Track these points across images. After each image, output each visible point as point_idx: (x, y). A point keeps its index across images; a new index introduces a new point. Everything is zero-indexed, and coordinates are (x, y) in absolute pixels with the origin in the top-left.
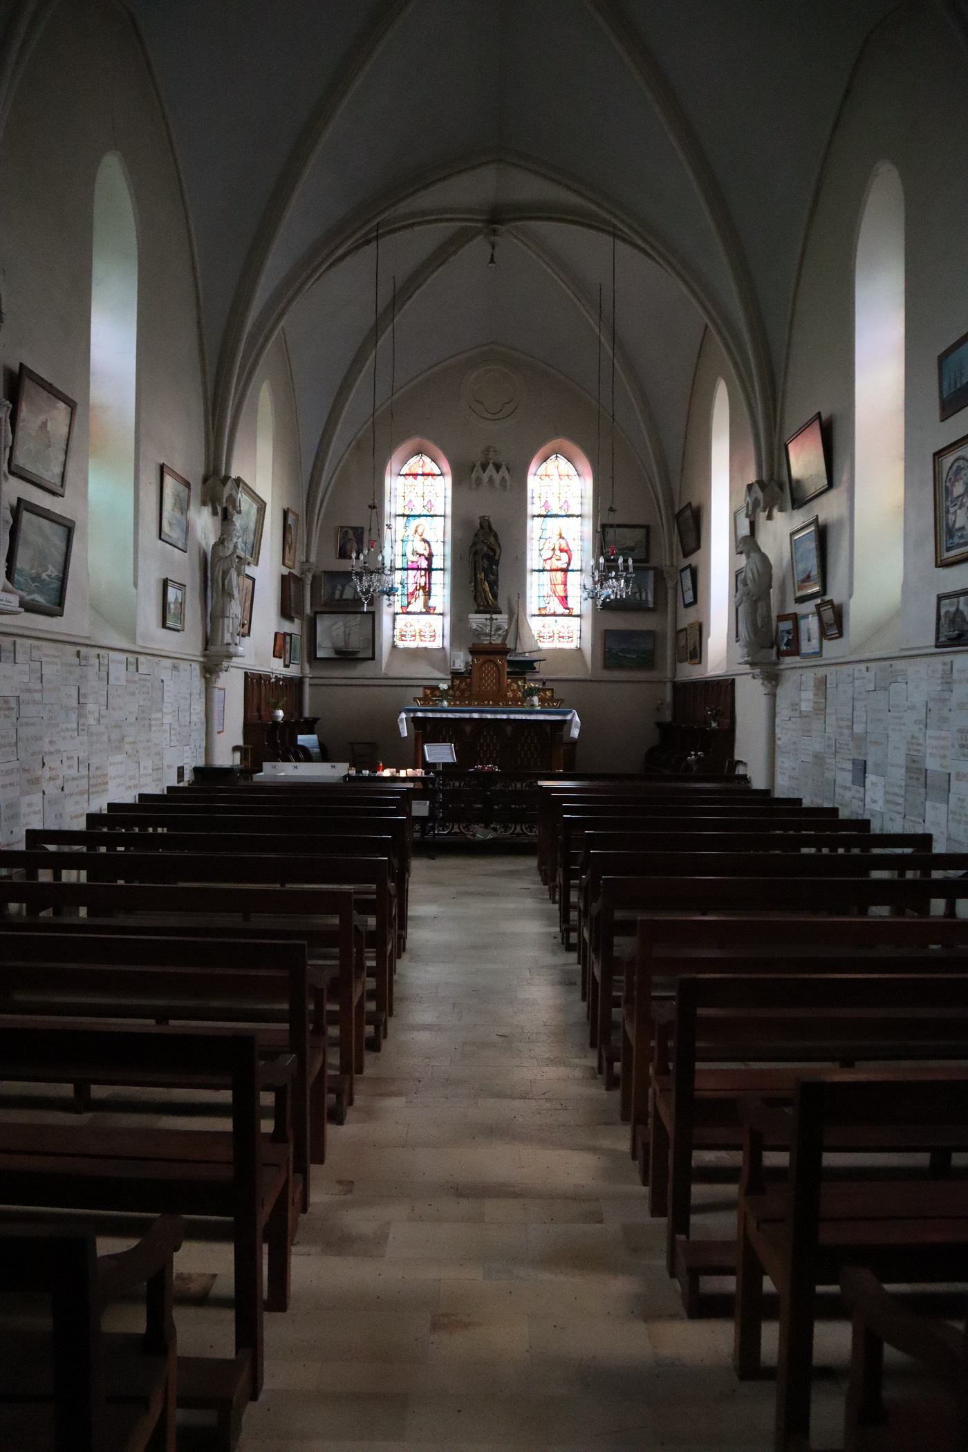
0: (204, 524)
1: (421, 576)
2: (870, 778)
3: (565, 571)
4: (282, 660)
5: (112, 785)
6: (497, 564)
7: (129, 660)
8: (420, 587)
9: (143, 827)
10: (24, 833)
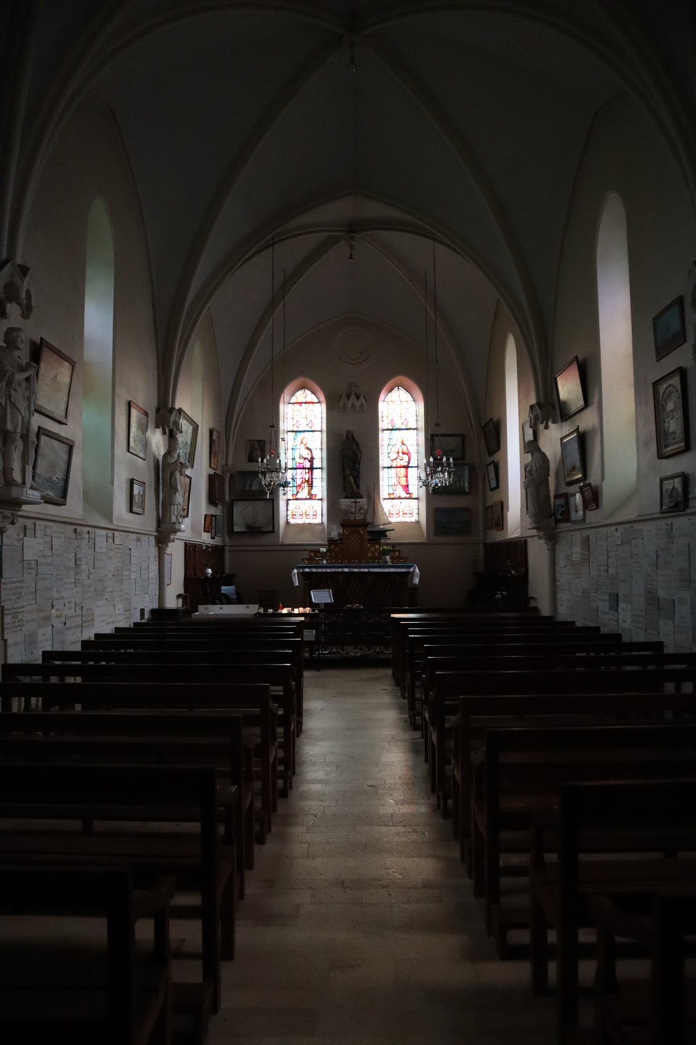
0: (157, 440)
1: (306, 473)
2: (622, 605)
3: (407, 467)
4: (210, 534)
5: (97, 621)
6: (359, 463)
7: (108, 535)
8: (305, 481)
9: (125, 650)
10: (41, 654)
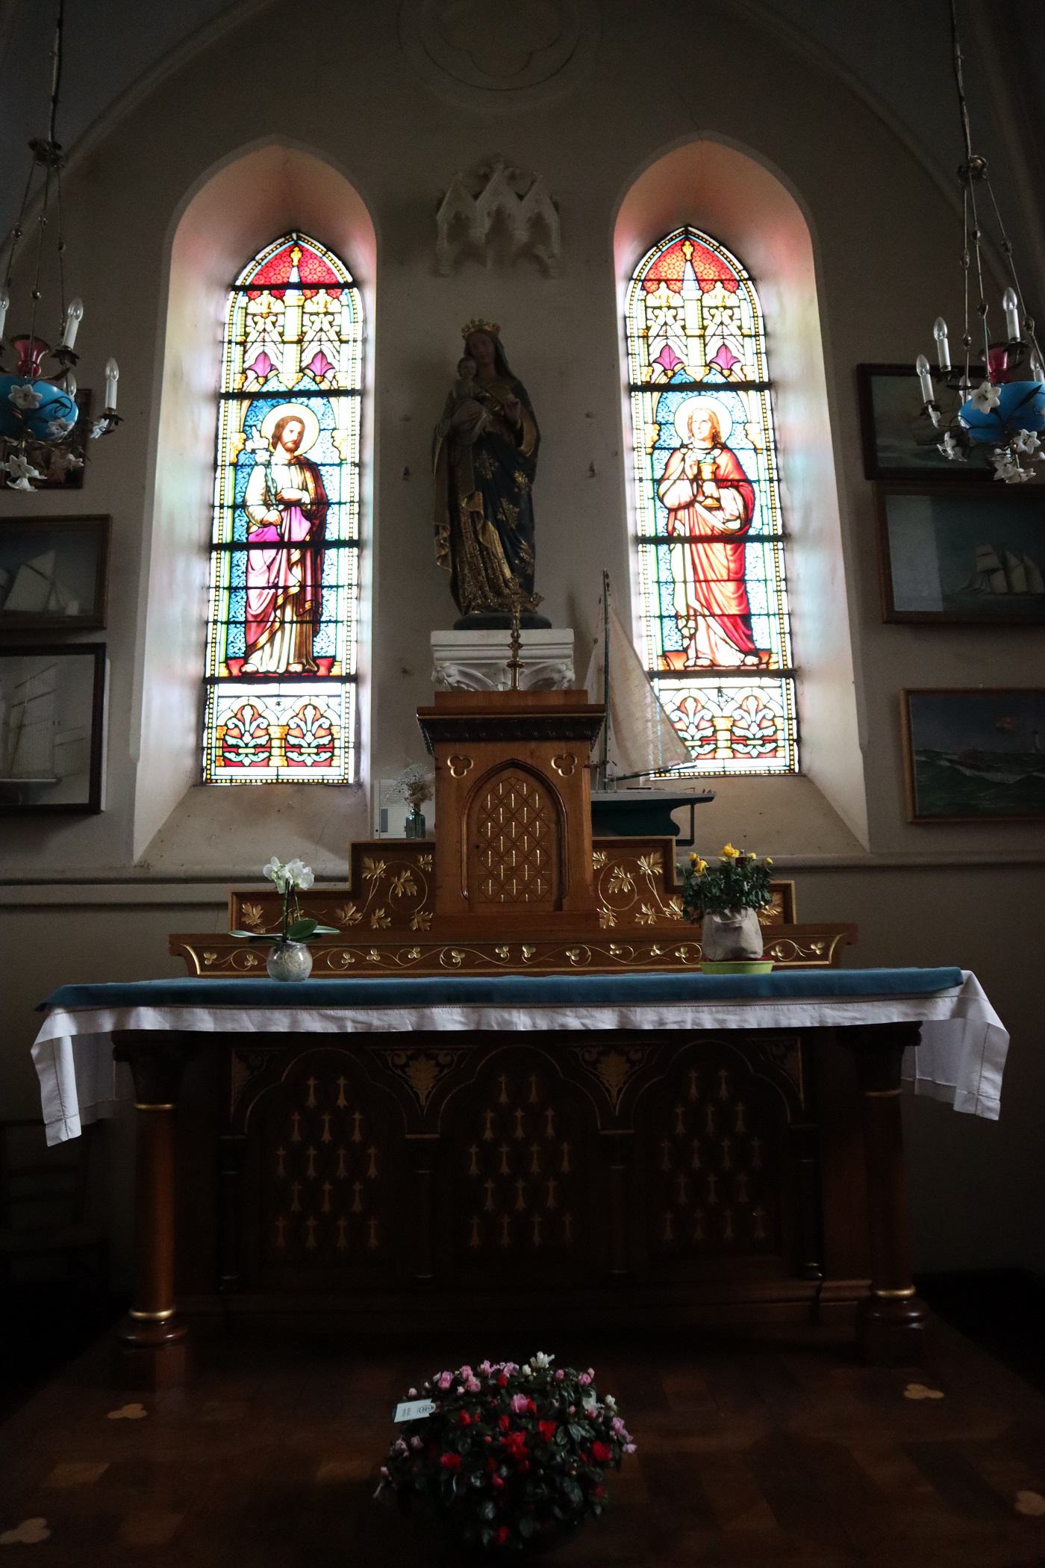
1: (290, 566)
8: (287, 598)
